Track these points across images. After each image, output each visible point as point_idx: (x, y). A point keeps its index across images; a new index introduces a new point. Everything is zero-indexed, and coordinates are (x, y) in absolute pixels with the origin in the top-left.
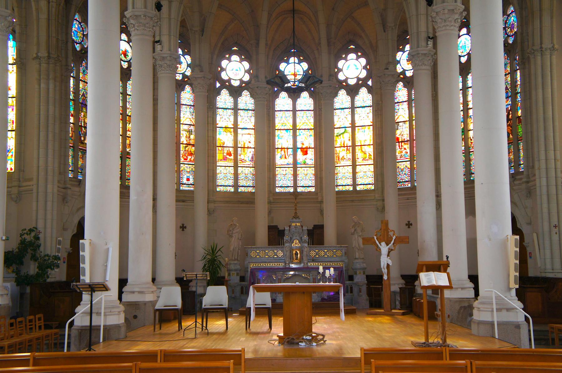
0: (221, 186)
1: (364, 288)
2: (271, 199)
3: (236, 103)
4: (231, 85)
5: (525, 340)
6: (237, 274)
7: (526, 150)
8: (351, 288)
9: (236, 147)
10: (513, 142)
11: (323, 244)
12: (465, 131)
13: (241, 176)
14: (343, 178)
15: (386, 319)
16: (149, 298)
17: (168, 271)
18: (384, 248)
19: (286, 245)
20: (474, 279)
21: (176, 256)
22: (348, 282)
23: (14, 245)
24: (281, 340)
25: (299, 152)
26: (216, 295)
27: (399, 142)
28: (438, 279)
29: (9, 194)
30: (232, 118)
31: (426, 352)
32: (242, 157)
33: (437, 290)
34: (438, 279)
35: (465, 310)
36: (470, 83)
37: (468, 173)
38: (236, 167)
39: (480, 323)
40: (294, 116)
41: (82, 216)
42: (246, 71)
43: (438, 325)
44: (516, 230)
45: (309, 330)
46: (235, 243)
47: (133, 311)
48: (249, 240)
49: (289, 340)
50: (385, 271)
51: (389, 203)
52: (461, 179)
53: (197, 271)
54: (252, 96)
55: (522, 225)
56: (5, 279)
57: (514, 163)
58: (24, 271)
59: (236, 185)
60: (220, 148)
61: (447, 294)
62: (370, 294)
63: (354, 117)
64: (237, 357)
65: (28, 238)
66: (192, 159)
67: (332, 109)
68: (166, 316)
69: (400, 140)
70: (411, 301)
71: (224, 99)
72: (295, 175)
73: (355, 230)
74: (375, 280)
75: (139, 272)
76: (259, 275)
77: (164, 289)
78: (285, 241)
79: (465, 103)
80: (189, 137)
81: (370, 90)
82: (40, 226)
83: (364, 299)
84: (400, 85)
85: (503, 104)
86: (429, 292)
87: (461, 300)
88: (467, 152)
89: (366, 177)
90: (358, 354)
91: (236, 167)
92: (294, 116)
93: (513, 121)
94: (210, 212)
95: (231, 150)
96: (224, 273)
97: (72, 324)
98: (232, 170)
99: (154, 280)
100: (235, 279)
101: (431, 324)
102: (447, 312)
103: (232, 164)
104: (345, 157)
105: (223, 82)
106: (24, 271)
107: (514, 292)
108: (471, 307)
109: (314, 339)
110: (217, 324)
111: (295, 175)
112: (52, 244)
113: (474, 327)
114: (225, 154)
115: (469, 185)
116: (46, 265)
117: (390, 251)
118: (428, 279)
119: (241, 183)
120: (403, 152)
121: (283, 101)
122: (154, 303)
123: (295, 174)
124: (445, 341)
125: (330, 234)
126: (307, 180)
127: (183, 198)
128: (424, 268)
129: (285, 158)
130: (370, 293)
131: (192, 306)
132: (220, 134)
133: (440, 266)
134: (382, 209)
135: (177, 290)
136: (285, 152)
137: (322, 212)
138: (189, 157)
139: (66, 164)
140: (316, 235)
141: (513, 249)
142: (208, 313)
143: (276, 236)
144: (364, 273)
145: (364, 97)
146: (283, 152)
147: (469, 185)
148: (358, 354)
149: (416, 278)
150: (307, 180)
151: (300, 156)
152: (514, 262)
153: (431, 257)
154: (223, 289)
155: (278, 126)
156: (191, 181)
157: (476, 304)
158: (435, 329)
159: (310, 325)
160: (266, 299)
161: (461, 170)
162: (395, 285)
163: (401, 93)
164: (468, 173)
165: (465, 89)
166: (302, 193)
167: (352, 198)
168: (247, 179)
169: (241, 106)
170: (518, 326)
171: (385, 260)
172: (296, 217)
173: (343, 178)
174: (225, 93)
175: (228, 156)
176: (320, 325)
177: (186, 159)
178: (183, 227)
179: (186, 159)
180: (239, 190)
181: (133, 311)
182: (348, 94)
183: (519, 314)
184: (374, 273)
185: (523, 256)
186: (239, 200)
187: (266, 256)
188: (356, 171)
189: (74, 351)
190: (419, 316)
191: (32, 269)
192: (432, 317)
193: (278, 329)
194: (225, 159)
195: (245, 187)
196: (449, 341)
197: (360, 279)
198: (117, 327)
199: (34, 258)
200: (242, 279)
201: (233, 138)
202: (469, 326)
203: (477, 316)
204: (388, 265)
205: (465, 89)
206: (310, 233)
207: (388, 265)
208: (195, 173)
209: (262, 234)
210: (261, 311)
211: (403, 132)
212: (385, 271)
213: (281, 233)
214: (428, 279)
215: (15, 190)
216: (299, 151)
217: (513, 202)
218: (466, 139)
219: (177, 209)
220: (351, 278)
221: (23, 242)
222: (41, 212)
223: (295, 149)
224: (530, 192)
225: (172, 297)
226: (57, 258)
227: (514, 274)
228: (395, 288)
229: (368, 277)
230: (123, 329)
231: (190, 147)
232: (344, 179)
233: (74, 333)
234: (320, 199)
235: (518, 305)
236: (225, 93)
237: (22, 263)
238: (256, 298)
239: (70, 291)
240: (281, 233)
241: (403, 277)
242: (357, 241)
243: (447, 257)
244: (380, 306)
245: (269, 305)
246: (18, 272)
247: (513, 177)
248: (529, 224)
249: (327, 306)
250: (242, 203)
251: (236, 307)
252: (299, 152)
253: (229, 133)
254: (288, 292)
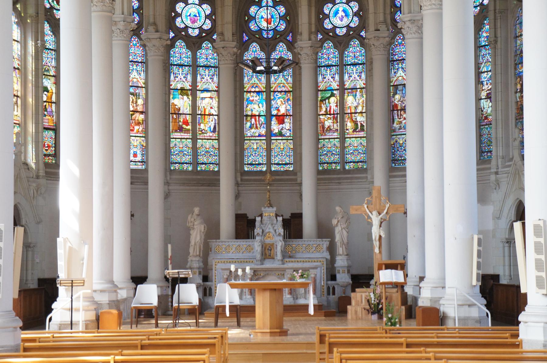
0: (203, 164)
2: (239, 179)
3: (195, 58)
4: (188, 36)
6: (200, 273)
8: (334, 288)
9: (194, 114)
11: (219, 239)
13: (201, 151)
19: (258, 238)
21: (131, 251)
25: (274, 121)
27: (398, 110)
30: (189, 77)
32: (202, 126)
38: (194, 139)
41: (166, 200)
42: (180, 15)
59: (195, 163)
60: (199, 116)
66: (140, 130)
69: (399, 108)
72: (269, 150)
73: (338, 222)
78: (256, 234)
80: (136, 102)
91: (194, 139)
95: (189, 118)
98: (189, 143)
103: (189, 135)
104: (332, 128)
111: (269, 150)
114: (180, 124)
119: (201, 159)
125: (309, 223)
128: (384, 267)
129: (257, 127)
132: (174, 98)
136: (256, 120)
138: (136, 128)
144: (349, 271)
146: (253, 120)
151: (275, 127)
155: (247, 87)
156: (139, 158)
166: (277, 173)
169: (201, 61)
175: (184, 126)
177: (133, 130)
179: (133, 130)
180: (273, 169)
182: (188, 47)
184: (47, 276)
194: (181, 129)
195: (205, 164)
201: (190, 103)
204: (380, 236)
206: (286, 224)
207: (380, 236)
209: (227, 223)
216: (274, 119)
231: (137, 115)
232: (329, 155)
234: (299, 181)
240: (251, 223)
250: (203, 185)
252: (274, 121)
253: (185, 97)
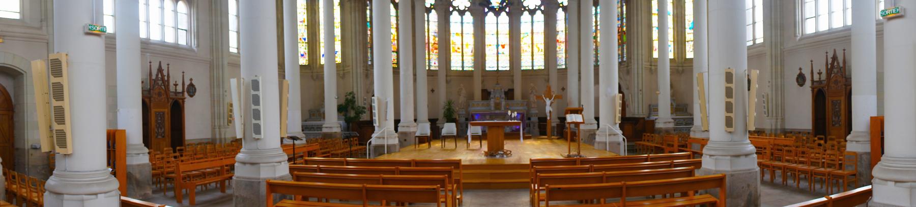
1: (537, 125)
5: (623, 152)
7: (627, 49)
10: (621, 45)
12: (595, 37)
14: (526, 64)
15: (547, 142)
16: (412, 130)
17: (424, 114)
18: (548, 102)
20: (597, 119)
22: (527, 121)
23: (343, 101)
24: (486, 154)
25: (500, 47)
26: (449, 128)
28: (577, 118)
29: (338, 74)
31: (569, 161)
33: (577, 124)
34: (577, 118)
35: (592, 136)
36: (599, 11)
37: (597, 61)
39: (599, 143)
40: (497, 26)
43: (576, 144)
44: (620, 92)
45: (502, 148)
46: (462, 99)
47: (404, 138)
48: (471, 97)
49: (490, 154)
50: (548, 115)
51: (549, 78)
52: (592, 64)
53: (441, 116)
54: (472, 15)
55: (624, 90)
56: (339, 119)
57: (621, 56)
58: (348, 115)
61: (582, 127)
62: (539, 128)
63: (532, 28)
64: (457, 164)
65: (350, 97)
67: (519, 22)
68: (422, 140)
70: (563, 132)
71: (455, 17)
74: (543, 120)
75: (407, 115)
76: (476, 117)
77: (420, 125)
79: (596, 22)
81: (543, 12)
82: (355, 91)
83: (537, 130)
84: (560, 10)
85: (617, 23)
86: (572, 126)
87: (590, 131)
88: (596, 50)
89: (540, 64)
90: (528, 162)
92: (497, 26)
93: (621, 33)
94: (447, 82)
96: (456, 116)
97: (370, 143)
99: (415, 120)
100: (463, 120)
101: (572, 144)
102: (581, 136)
105: (454, 8)
106: (348, 115)
107: (618, 125)
108: (595, 134)
109: (505, 153)
110: (450, 145)
112: (360, 102)
113: (596, 145)
115: (596, 67)
116: (359, 112)
117: (551, 103)
118: (571, 118)
120: (561, 48)
121: (490, 18)
122: (415, 133)
123: (497, 60)
124: (579, 153)
125: (518, 93)
126: (505, 65)
127: (431, 74)
130: (540, 127)
131: (436, 134)
133: (578, 111)
134: (548, 81)
135: (428, 126)
137: (513, 82)
139: (367, 57)
140: (510, 94)
141: (619, 102)
142: (445, 138)
143: (486, 94)
145: (539, 17)
147: (596, 67)
148: (528, 162)
149: (565, 119)
150: (505, 65)
152: (619, 108)
153: (575, 106)
154: (454, 125)
157: (597, 132)
158: (574, 146)
159: (503, 145)
160: (478, 130)
161: (593, 59)
162: (554, 122)
163: (561, 14)
164: (597, 61)
165: (596, 14)
167: (531, 74)
168: (469, 65)
170: (619, 144)
171: (548, 109)
172: (497, 84)
173: (526, 64)
174: (455, 13)
176: (508, 145)
178: (433, 91)
181: (404, 138)
183: (620, 137)
185: (624, 105)
186: (464, 75)
187: (478, 106)
188: (533, 58)
189: (372, 158)
190: (567, 140)
191: (352, 114)
192: (572, 140)
193: (485, 148)
196: (582, 153)
197: (535, 119)
198: (394, 145)
199: (353, 108)
200: (467, 119)
202: (593, 145)
203: (598, 139)
205: (596, 14)
206: (506, 93)
208: (439, 59)
209: (478, 94)
210: (475, 138)
211: (561, 37)
212: (548, 115)
213: (489, 93)
214: (571, 118)
215: (342, 72)
217: (620, 77)
218: (596, 42)
219: (428, 80)
220: (529, 119)
221: (347, 100)
222: (355, 85)
223: (498, 46)
224: (628, 72)
225: (425, 129)
226: (364, 108)
227: (619, 115)
228: (554, 124)
229: (539, 118)
230: (398, 147)
233: (372, 148)
235: (620, 132)
236: (455, 13)
237: (347, 111)
238: (472, 130)
239: (369, 127)
240: (489, 93)
241: (559, 118)
242: (533, 98)
243: (191, 80)
244: (545, 135)
245: (480, 134)
246: (345, 115)
247: (620, 64)
248: (628, 89)
249: (513, 135)
251: (461, 135)
254: (491, 126)
